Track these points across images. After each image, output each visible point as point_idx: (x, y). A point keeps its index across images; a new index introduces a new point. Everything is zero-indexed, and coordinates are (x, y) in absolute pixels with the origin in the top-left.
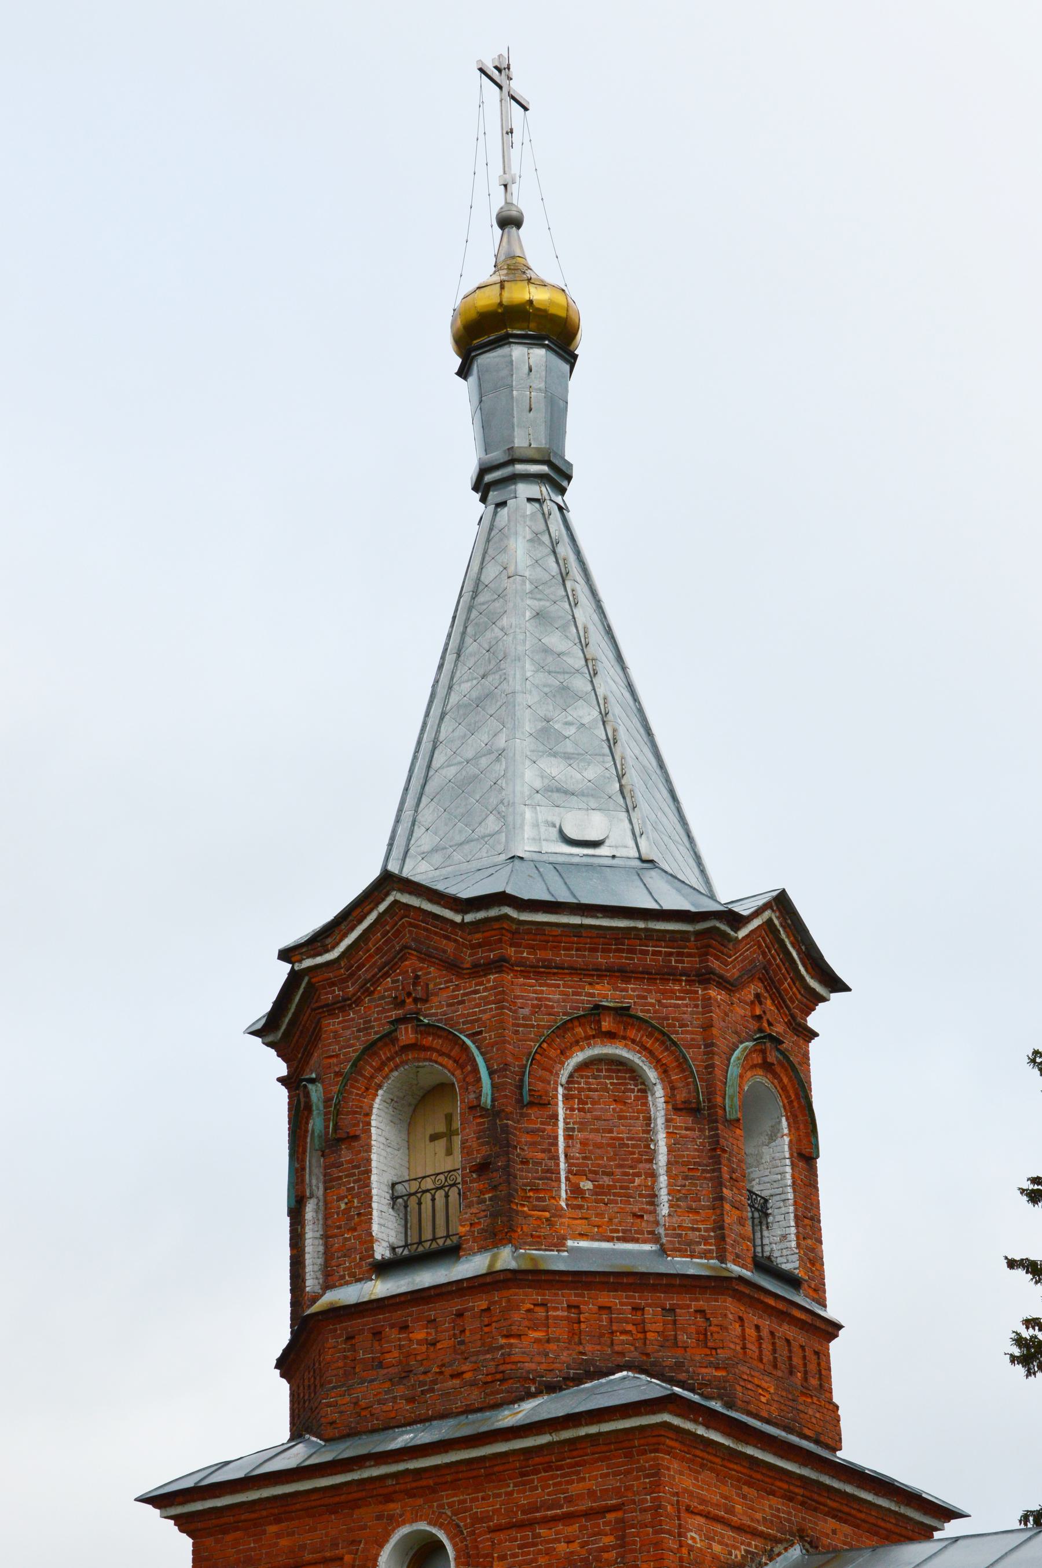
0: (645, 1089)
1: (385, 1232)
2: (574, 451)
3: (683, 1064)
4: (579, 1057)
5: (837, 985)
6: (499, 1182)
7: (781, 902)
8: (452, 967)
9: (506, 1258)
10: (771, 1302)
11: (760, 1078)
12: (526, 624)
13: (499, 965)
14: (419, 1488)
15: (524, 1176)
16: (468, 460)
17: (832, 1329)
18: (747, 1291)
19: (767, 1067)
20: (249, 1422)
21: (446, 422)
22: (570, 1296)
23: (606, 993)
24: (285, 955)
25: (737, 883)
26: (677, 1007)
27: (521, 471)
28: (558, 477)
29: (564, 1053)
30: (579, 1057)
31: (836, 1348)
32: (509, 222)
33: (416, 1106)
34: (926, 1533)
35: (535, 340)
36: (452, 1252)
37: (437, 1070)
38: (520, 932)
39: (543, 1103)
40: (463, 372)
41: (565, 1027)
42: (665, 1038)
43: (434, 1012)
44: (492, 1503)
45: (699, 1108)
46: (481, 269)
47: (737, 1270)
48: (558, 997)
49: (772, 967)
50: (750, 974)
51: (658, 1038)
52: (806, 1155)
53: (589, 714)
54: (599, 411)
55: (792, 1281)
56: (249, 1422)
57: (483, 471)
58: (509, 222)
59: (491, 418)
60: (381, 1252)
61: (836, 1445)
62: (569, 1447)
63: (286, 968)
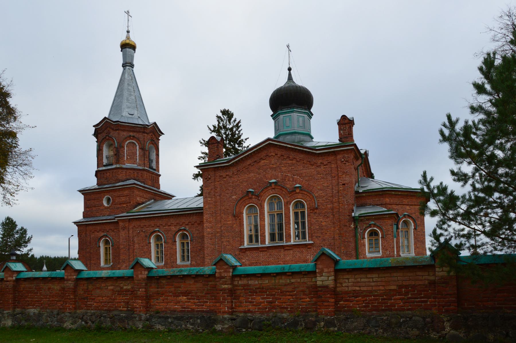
0: (136, 146)
1: (105, 161)
2: (135, 63)
3: (141, 143)
4: (128, 142)
5: (163, 134)
6: (118, 156)
7: (155, 123)
8: (113, 129)
9: (118, 166)
11: (152, 145)
12: (290, 78)
13: (118, 130)
14: (108, 192)
15: (120, 156)
16: (121, 62)
17: (160, 175)
19: (152, 144)
20: (92, 182)
21: (118, 57)
22: (125, 171)
23: (132, 134)
24: (94, 126)
26: (140, 136)
27: (128, 64)
28: (132, 66)
29: (126, 141)
30: (128, 142)
31: (160, 178)
32: (128, 32)
33: (110, 146)
34: (171, 199)
35: (130, 48)
36: (112, 165)
37: (111, 142)
38: (121, 126)
39: (124, 147)
40: (121, 51)
41: (126, 138)
42: (139, 141)
43: (111, 135)
44: (116, 194)
45: (142, 149)
47: (146, 168)
48: (125, 134)
50: (151, 132)
51: (138, 140)
52: (158, 155)
53: (133, 98)
54: (138, 58)
55: (155, 170)
56: (92, 182)
57: (123, 64)
58: (128, 32)
59: (124, 57)
60: (104, 164)
62: (123, 188)
63: (94, 128)
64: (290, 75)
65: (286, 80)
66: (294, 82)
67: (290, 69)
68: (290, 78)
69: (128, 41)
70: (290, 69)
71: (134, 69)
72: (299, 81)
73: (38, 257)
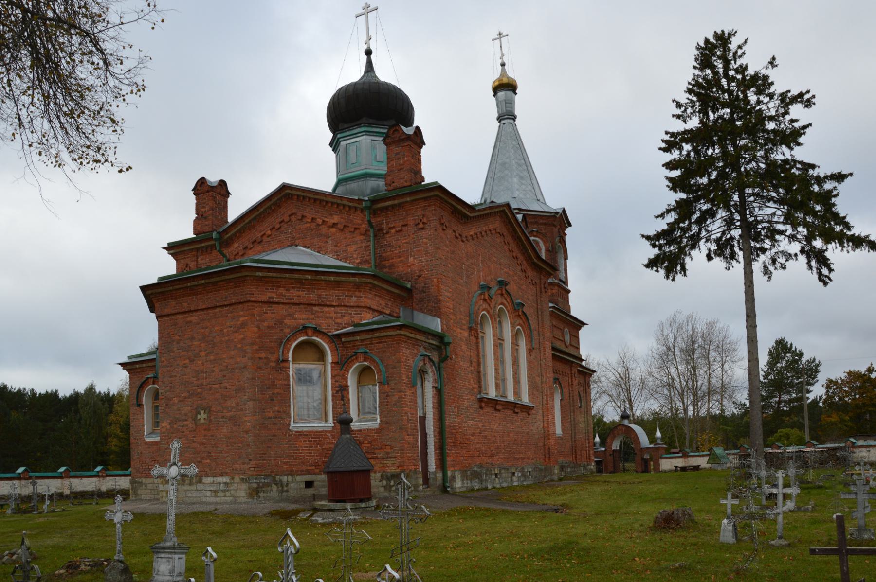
7: (564, 211)
12: (369, 66)
17: (569, 291)
21: (490, 107)
27: (507, 115)
28: (514, 118)
32: (503, 65)
49: (559, 221)
52: (566, 258)
54: (521, 103)
58: (503, 65)
64: (369, 64)
66: (376, 77)
68: (369, 66)
69: (505, 80)
72: (384, 74)
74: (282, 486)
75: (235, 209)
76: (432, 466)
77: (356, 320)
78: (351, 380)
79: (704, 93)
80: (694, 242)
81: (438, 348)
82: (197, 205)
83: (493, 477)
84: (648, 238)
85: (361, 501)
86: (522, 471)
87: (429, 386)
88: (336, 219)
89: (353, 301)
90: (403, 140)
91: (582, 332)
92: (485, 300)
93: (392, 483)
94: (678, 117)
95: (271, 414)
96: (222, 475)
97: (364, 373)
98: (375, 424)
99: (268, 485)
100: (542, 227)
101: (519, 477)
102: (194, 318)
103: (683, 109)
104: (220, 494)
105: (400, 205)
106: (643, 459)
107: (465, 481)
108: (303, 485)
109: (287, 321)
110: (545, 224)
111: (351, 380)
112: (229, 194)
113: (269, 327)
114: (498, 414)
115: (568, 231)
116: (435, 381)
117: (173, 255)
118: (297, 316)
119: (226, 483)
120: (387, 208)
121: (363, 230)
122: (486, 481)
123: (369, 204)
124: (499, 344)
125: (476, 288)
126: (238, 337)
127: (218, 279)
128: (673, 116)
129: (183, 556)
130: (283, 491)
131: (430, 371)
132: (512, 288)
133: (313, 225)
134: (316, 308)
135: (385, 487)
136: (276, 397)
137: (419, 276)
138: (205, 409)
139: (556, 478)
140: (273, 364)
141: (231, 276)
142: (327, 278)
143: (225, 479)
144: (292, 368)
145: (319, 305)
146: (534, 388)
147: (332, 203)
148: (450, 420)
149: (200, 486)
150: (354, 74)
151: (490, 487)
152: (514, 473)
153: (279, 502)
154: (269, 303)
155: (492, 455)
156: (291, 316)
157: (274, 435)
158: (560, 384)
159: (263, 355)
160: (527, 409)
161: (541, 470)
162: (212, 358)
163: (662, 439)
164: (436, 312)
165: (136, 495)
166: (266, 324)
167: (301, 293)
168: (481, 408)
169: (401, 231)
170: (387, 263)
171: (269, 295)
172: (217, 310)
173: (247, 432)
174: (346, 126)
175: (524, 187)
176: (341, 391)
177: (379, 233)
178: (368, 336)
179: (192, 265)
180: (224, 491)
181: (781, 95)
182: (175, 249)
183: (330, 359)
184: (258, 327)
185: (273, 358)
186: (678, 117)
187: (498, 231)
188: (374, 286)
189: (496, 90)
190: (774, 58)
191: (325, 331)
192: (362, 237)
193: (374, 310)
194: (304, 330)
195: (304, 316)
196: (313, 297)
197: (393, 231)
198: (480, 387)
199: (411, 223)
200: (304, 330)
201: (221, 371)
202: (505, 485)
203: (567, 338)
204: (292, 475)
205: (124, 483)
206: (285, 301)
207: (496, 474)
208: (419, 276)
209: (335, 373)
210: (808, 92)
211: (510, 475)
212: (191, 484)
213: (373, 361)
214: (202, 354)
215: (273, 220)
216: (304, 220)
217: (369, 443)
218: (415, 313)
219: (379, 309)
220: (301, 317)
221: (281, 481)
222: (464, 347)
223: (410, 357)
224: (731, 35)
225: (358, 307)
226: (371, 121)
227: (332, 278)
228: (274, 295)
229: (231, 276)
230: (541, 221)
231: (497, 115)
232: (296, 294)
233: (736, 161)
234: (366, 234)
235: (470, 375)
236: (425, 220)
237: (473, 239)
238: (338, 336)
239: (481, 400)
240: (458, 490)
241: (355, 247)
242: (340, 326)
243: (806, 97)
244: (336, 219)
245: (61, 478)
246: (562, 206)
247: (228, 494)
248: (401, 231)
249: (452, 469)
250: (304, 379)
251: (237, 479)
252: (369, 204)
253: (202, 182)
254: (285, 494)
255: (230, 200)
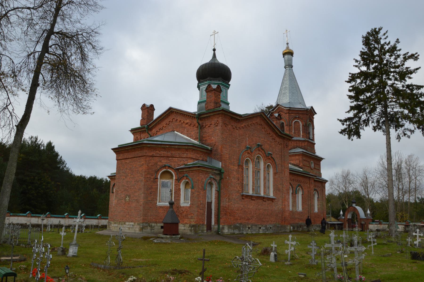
7: (312, 107)
10: (191, 166)
12: (214, 55)
17: (315, 144)
18: (204, 170)
21: (281, 61)
25: (308, 105)
27: (289, 66)
28: (292, 67)
31: (315, 145)
46: (285, 49)
49: (311, 112)
52: (313, 129)
54: (295, 60)
61: (315, 153)
65: (211, 58)
67: (214, 50)
70: (214, 50)
71: (293, 69)
72: (221, 59)
73: (89, 177)
74: (152, 227)
75: (156, 114)
76: (213, 223)
77: (186, 163)
78: (182, 187)
79: (366, 58)
80: (366, 122)
81: (219, 174)
82: (142, 114)
83: (247, 229)
84: (341, 121)
85: (173, 235)
86: (266, 227)
87: (214, 189)
88: (188, 121)
89: (185, 155)
90: (212, 91)
91: (322, 162)
92: (248, 153)
93: (193, 229)
94: (356, 66)
95: (150, 199)
96: (132, 222)
97: (187, 184)
98: (188, 205)
99: (147, 227)
100: (301, 115)
101: (263, 230)
102: (128, 161)
103: (358, 63)
104: (131, 229)
105: (209, 116)
106: (361, 224)
107: (230, 230)
108: (160, 228)
109: (159, 163)
110: (302, 114)
111: (182, 187)
112: (154, 109)
113: (152, 166)
114: (253, 201)
115: (315, 116)
116: (216, 188)
117: (133, 133)
118: (163, 161)
119: (133, 225)
120: (205, 117)
121: (197, 126)
122: (243, 230)
123: (198, 116)
124: (256, 172)
125: (244, 148)
126: (141, 169)
127: (135, 147)
128: (354, 66)
129: (77, 247)
130: (152, 229)
131: (214, 184)
132: (266, 147)
133: (180, 123)
134: (170, 158)
135: (190, 230)
136: (151, 192)
137: (215, 145)
138: (128, 196)
139: (288, 231)
140: (152, 180)
141: (139, 146)
142: (174, 147)
143: (132, 223)
144: (159, 181)
145: (171, 157)
146: (276, 189)
147: (187, 115)
148: (224, 203)
149: (125, 226)
150: (207, 59)
151: (245, 233)
152: (260, 228)
153: (150, 233)
154: (152, 156)
155: (248, 219)
156: (161, 161)
157: (151, 207)
158: (301, 187)
159: (149, 176)
160: (272, 200)
161: (278, 227)
162: (132, 176)
163: (370, 215)
164: (220, 159)
165: (109, 227)
166: (150, 164)
167: (165, 153)
168: (243, 199)
169: (209, 126)
170: (204, 139)
171: (153, 153)
172: (135, 158)
173: (141, 206)
174: (202, 80)
175: (294, 97)
176: (178, 191)
177: (202, 127)
178: (188, 170)
179: (139, 137)
180: (132, 228)
181: (404, 55)
182: (134, 131)
183: (174, 178)
184: (148, 165)
185: (152, 177)
186: (356, 66)
187: (258, 123)
188: (194, 150)
189: (284, 54)
190: (398, 39)
191: (173, 167)
192: (197, 129)
193: (194, 159)
194: (165, 167)
195: (165, 161)
196: (169, 154)
197: (207, 126)
198: (243, 190)
199: (213, 123)
200: (165, 167)
201: (135, 181)
202: (254, 232)
203: (313, 166)
204: (156, 223)
205: (104, 222)
206: (158, 155)
207: (249, 228)
208: (215, 145)
209: (176, 183)
210: (417, 53)
211: (258, 228)
212: (122, 225)
213: (189, 179)
214: (129, 175)
215: (167, 121)
216: (178, 121)
217: (186, 212)
218: (213, 159)
219: (197, 158)
220: (164, 162)
221: (152, 225)
222: (235, 173)
223: (205, 178)
224: (380, 29)
225: (187, 158)
226: (211, 78)
227: (176, 147)
228: (154, 153)
229: (139, 146)
230: (300, 112)
231: (284, 66)
232: (163, 153)
233: (378, 89)
234: (197, 127)
235: (237, 185)
236: (218, 123)
237: (243, 128)
238: (178, 169)
239: (243, 195)
240: (225, 233)
241: (194, 132)
242: (179, 165)
243: (416, 56)
244: (188, 121)
245: (98, 219)
246: (311, 105)
247: (133, 229)
248: (209, 126)
249: (223, 224)
250: (164, 185)
251: (136, 224)
252: (198, 116)
253: (144, 105)
254: (153, 230)
255: (155, 112)
